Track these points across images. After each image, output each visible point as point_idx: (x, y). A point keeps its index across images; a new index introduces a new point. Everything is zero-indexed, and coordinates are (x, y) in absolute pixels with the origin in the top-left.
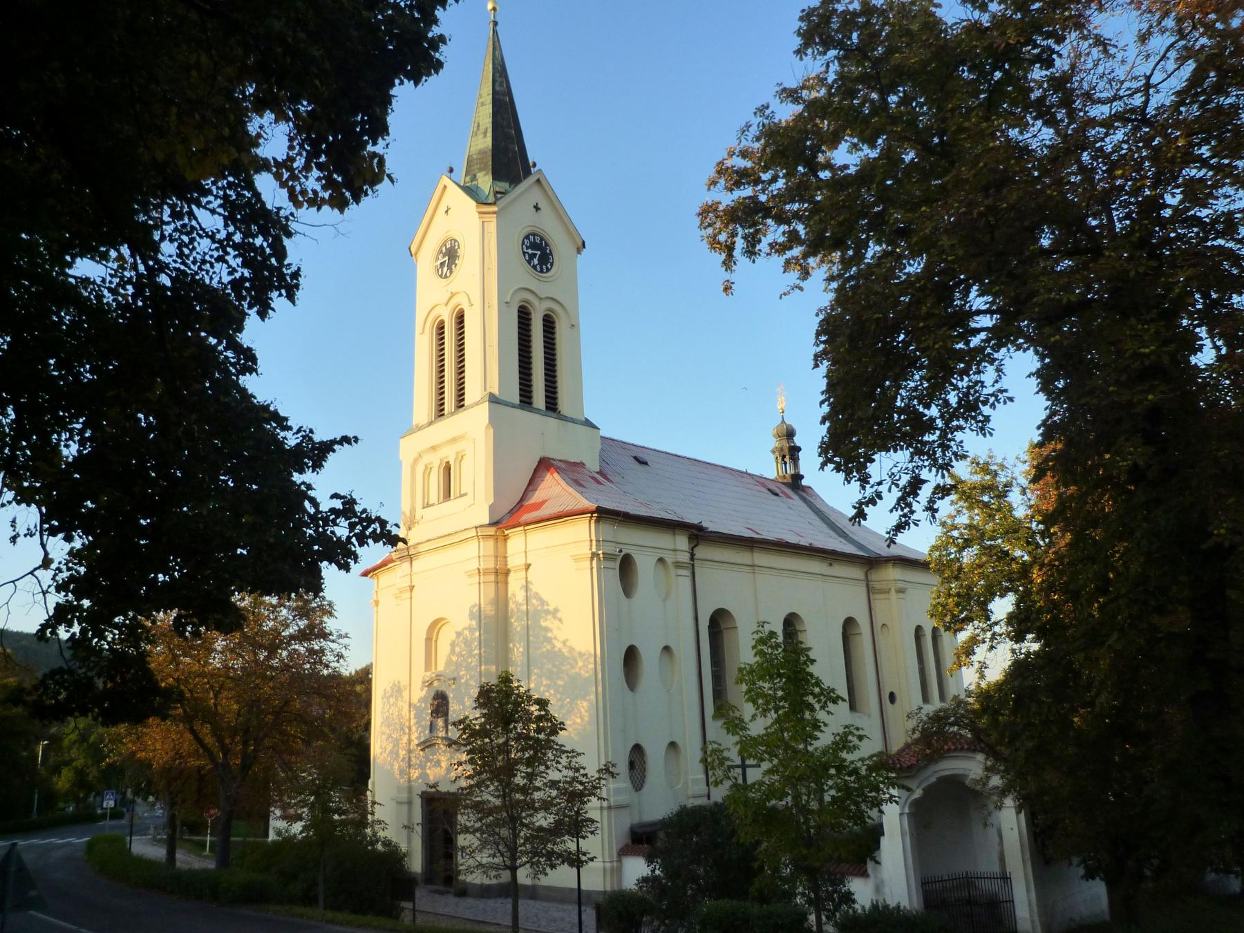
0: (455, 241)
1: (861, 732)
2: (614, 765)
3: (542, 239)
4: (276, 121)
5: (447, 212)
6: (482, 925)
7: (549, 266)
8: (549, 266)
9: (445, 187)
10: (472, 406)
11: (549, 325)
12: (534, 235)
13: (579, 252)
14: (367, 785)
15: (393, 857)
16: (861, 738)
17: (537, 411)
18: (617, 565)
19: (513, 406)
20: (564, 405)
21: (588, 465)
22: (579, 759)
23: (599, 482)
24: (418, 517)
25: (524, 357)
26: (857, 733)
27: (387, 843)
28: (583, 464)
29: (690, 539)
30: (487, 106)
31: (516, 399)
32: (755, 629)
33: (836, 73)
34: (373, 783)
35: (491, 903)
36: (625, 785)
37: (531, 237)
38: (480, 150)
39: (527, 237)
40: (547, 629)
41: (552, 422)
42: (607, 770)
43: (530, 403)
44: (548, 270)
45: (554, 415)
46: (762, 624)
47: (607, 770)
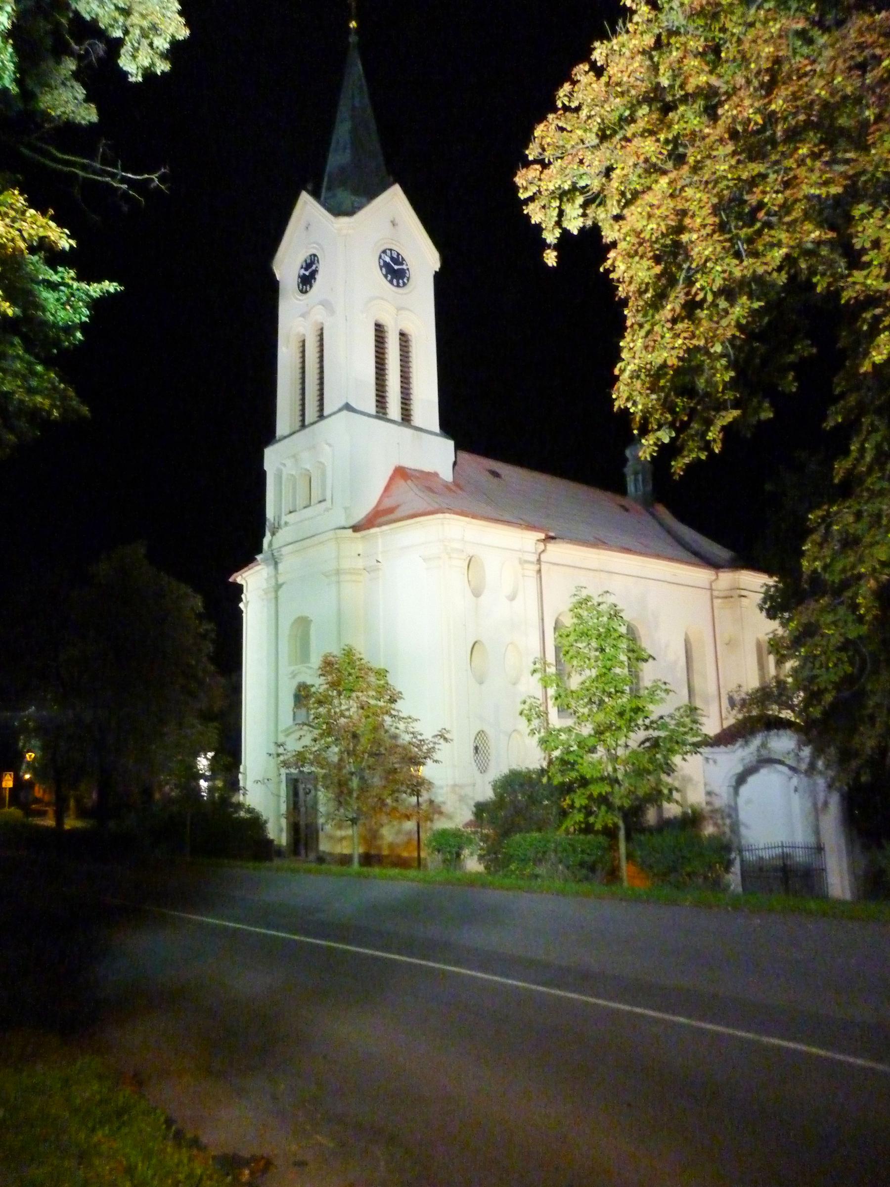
1: (668, 687)
2: (448, 732)
3: (398, 254)
4: (540, 223)
7: (405, 280)
8: (405, 280)
10: (330, 416)
14: (238, 768)
15: (256, 823)
16: (667, 691)
19: (369, 415)
22: (414, 724)
24: (282, 523)
25: (405, 388)
26: (664, 687)
27: (250, 810)
31: (372, 408)
32: (574, 592)
33: (879, 14)
34: (245, 769)
41: (406, 431)
42: (442, 736)
43: (385, 414)
44: (404, 284)
46: (580, 588)
47: (442, 736)
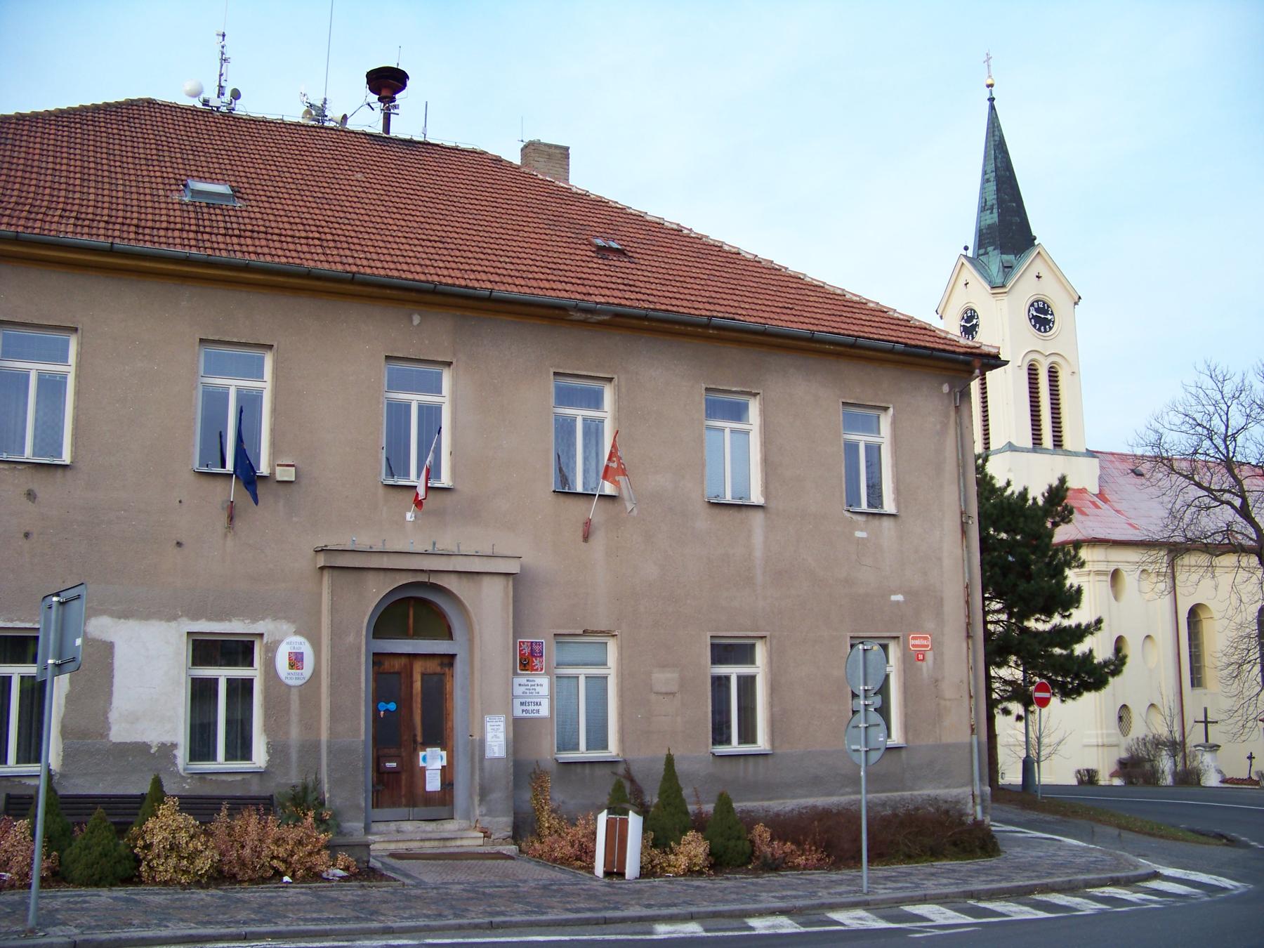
0: (975, 312)
3: (1044, 303)
5: (966, 284)
6: (594, 475)
7: (1051, 325)
9: (963, 264)
11: (1053, 375)
12: (1037, 301)
13: (1076, 303)
17: (1046, 451)
18: (1109, 578)
19: (1028, 451)
20: (1068, 444)
21: (1089, 489)
23: (1097, 507)
28: (1086, 489)
29: (1170, 551)
30: (992, 183)
31: (1030, 445)
35: (1236, 497)
36: (1114, 731)
37: (1036, 304)
38: (989, 225)
39: (1032, 305)
40: (1071, 586)
44: (1051, 328)
45: (1061, 452)
